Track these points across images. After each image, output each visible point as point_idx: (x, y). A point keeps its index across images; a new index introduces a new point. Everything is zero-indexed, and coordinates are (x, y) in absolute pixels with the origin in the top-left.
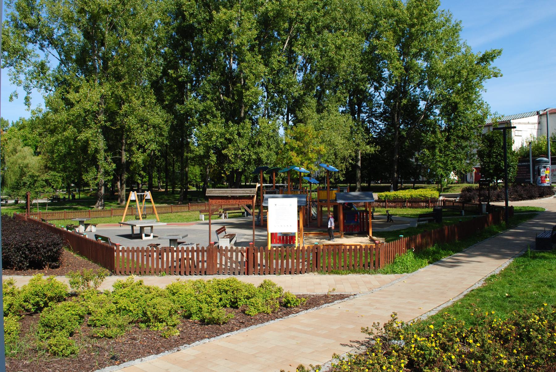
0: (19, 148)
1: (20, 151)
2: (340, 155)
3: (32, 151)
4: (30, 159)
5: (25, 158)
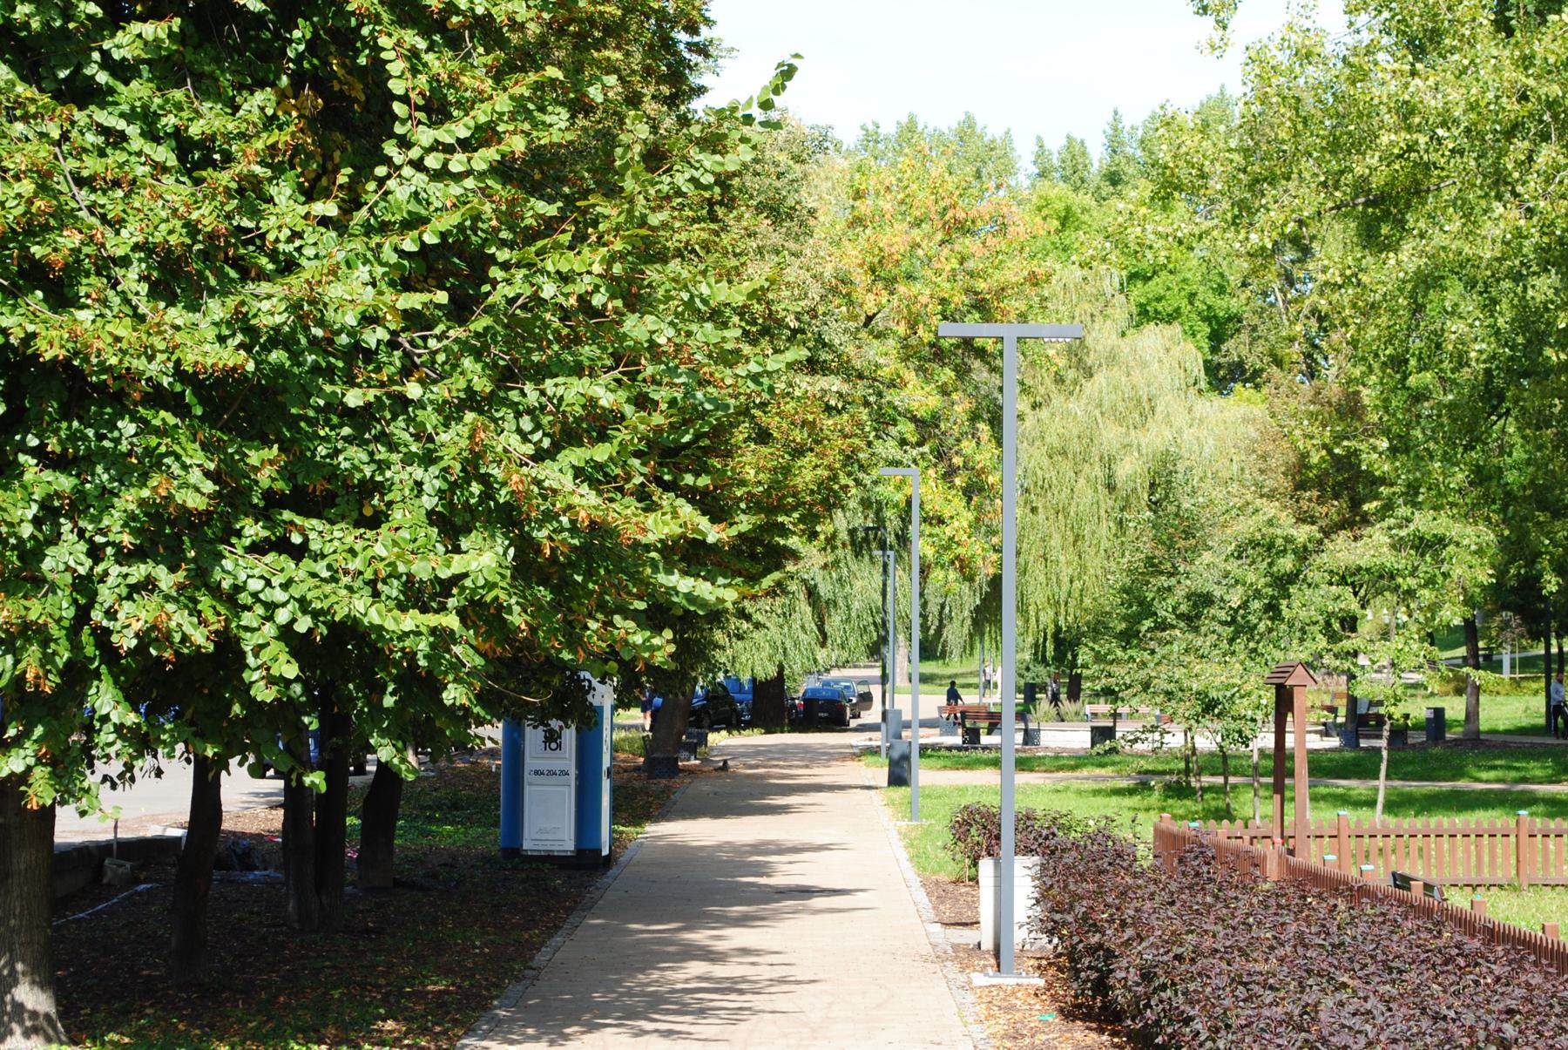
0: (1103, 337)
1: (1112, 358)
2: (515, 455)
3: (1192, 355)
4: (1180, 419)
5: (1144, 409)
